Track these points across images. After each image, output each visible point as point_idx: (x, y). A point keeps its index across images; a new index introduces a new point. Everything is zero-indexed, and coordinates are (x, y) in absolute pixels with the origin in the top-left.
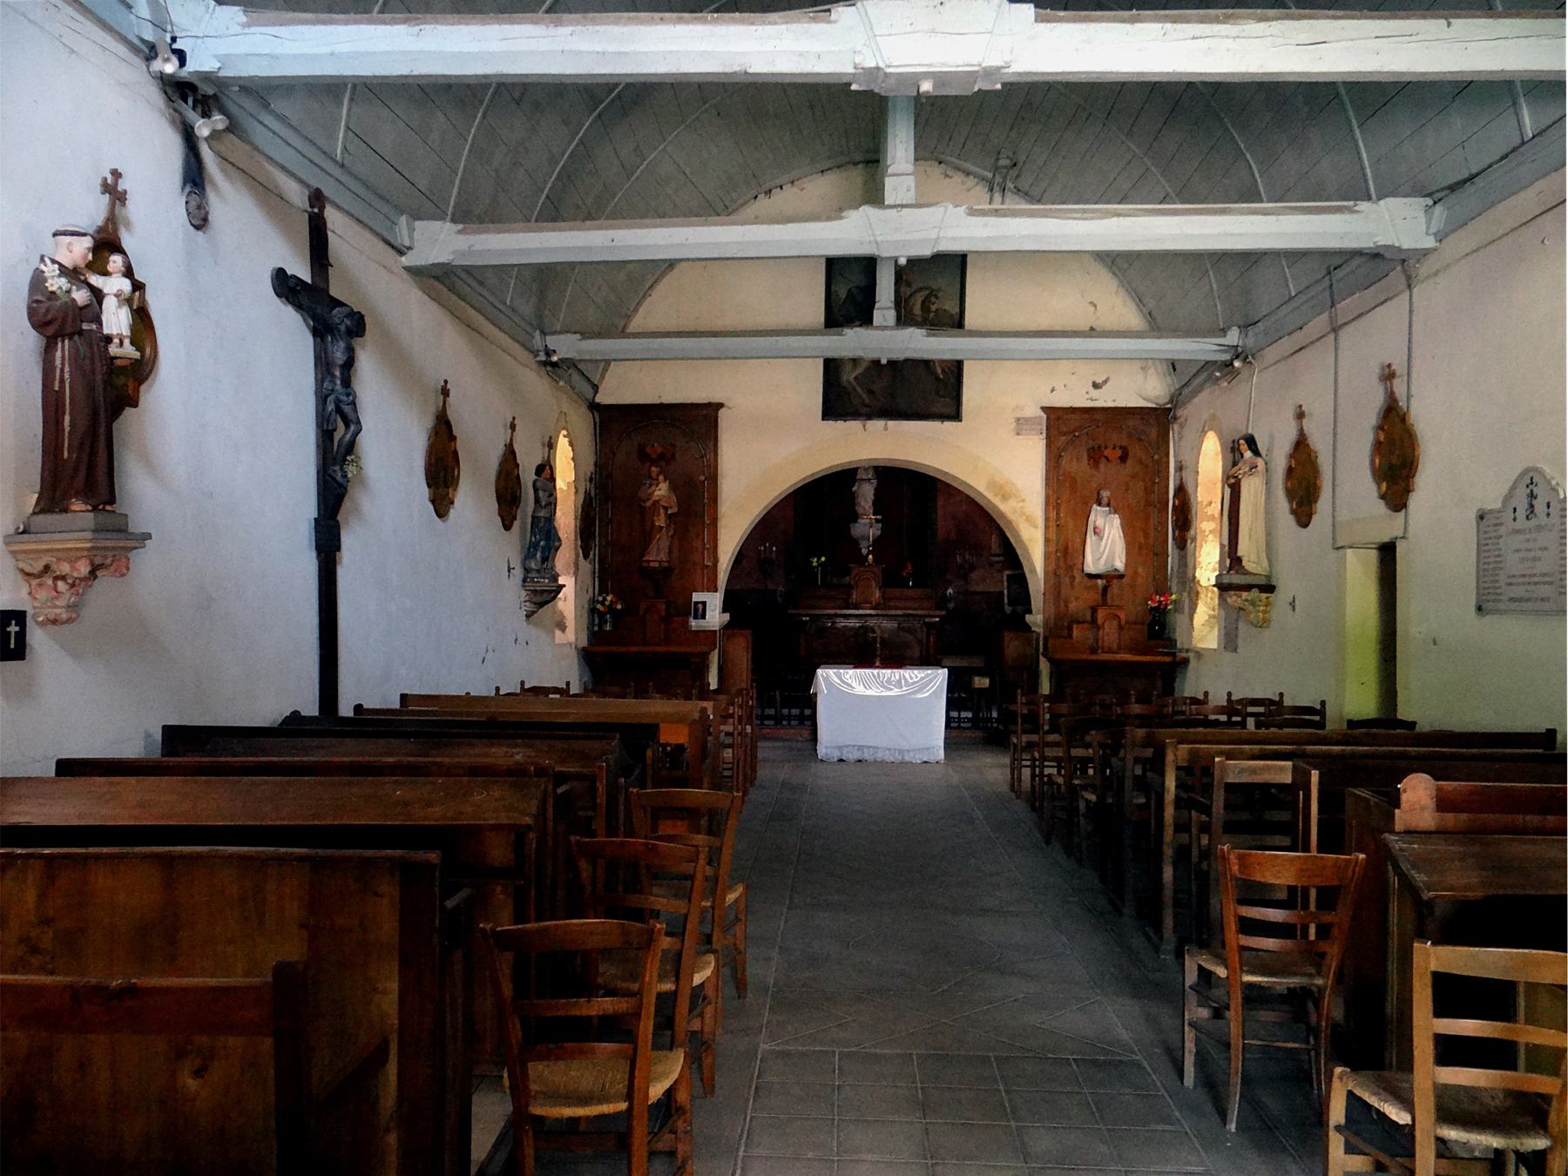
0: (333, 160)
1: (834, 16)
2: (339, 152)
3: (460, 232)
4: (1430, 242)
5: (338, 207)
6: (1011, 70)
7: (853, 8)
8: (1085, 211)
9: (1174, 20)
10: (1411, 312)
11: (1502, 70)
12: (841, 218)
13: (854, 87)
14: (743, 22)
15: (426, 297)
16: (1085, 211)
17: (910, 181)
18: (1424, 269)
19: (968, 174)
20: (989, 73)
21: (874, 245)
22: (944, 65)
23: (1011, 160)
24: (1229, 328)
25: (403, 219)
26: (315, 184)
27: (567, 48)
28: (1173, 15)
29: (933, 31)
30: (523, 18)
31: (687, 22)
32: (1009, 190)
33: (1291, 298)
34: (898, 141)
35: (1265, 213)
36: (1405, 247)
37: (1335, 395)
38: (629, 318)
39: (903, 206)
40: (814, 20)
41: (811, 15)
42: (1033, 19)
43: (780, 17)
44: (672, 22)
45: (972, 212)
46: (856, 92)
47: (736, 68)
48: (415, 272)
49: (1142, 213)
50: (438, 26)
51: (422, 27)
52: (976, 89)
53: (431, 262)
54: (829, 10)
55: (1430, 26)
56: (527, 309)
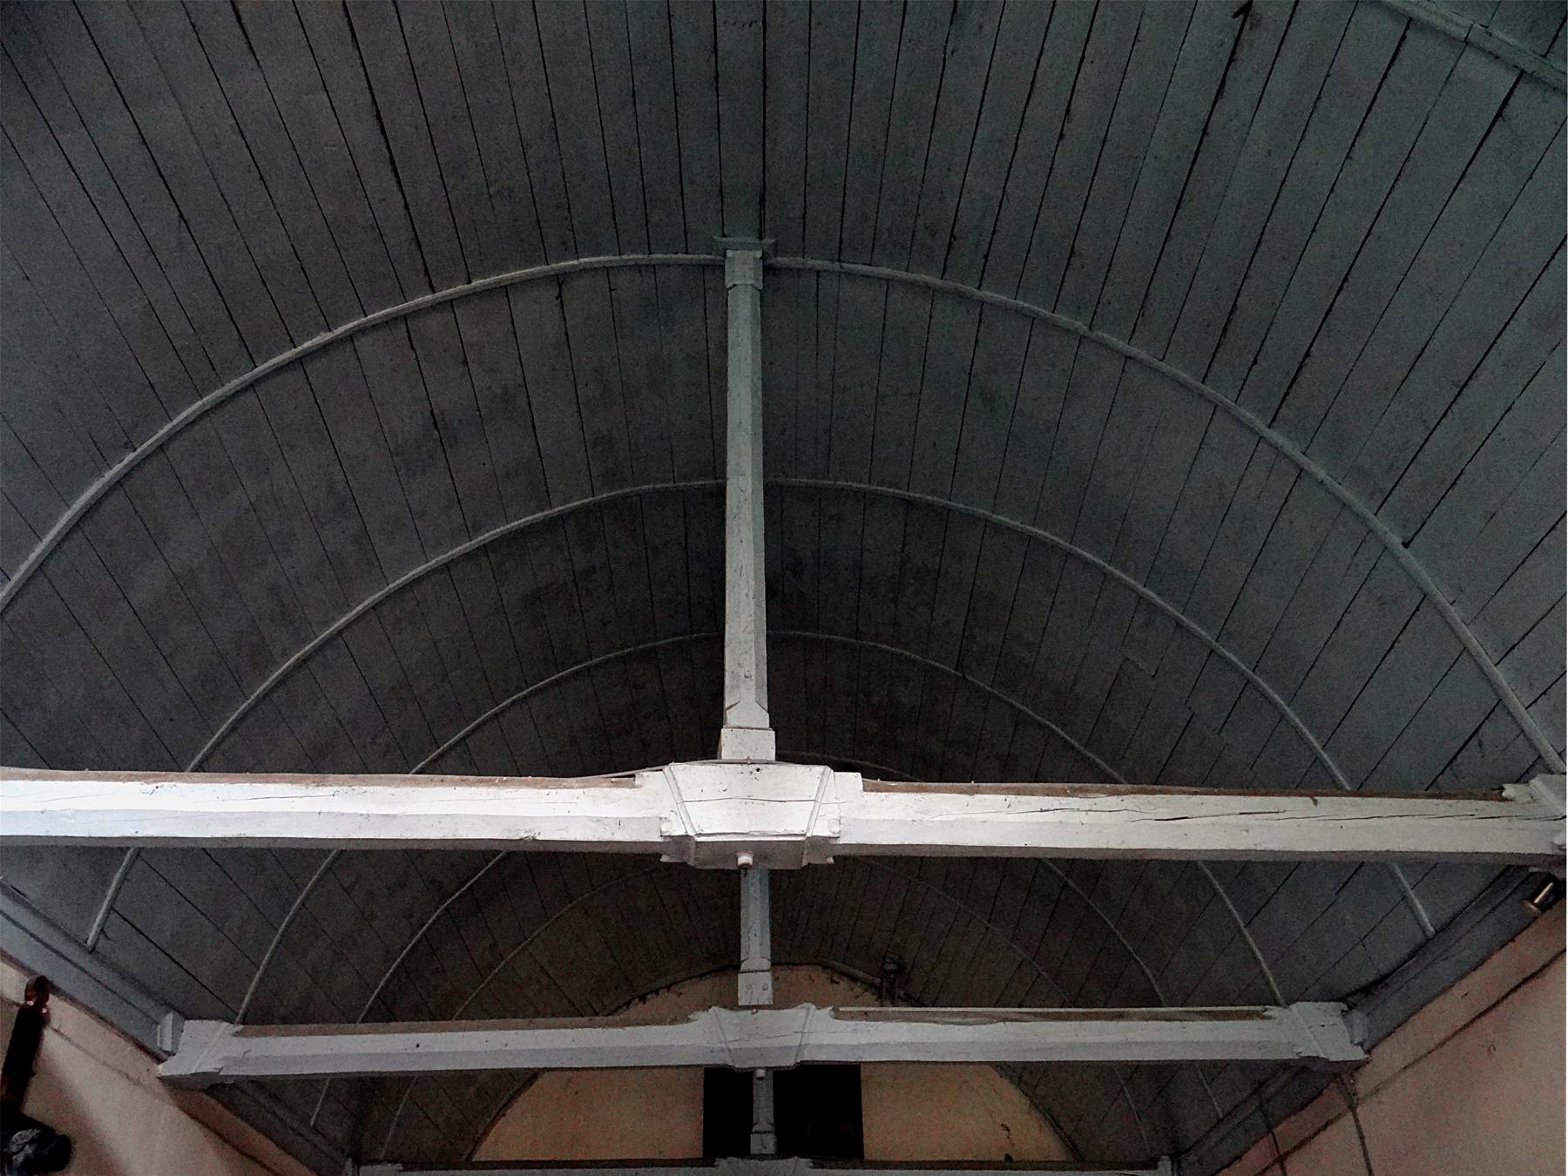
0: (81, 944)
1: (638, 782)
2: (92, 934)
3: (237, 1034)
4: (1358, 1054)
5: (72, 1000)
6: (841, 842)
7: (661, 772)
8: (966, 1014)
9: (1018, 793)
10: (1362, 1138)
11: (1388, 851)
12: (688, 1020)
13: (664, 859)
14: (535, 785)
15: (184, 1117)
16: (966, 1014)
17: (767, 978)
18: (1363, 1084)
19: (855, 979)
20: (817, 843)
21: (727, 1053)
22: (764, 834)
23: (898, 965)
24: (1159, 1159)
25: (169, 1018)
26: (42, 969)
27: (325, 810)
28: (1015, 788)
29: (749, 798)
30: (281, 778)
31: (470, 784)
32: (899, 997)
33: (1220, 1121)
34: (751, 935)
35: (1169, 1018)
36: (1333, 1059)
37: (1478, 149)
38: (477, 1142)
39: (759, 1007)
40: (617, 785)
41: (613, 780)
42: (862, 788)
43: (577, 782)
44: (455, 784)
45: (838, 1016)
46: (669, 866)
47: (523, 835)
48: (175, 1085)
49: (1026, 1017)
50: (178, 784)
51: (159, 784)
52: (805, 863)
53: (193, 1072)
54: (633, 776)
55: (1297, 805)
56: (338, 1132)
